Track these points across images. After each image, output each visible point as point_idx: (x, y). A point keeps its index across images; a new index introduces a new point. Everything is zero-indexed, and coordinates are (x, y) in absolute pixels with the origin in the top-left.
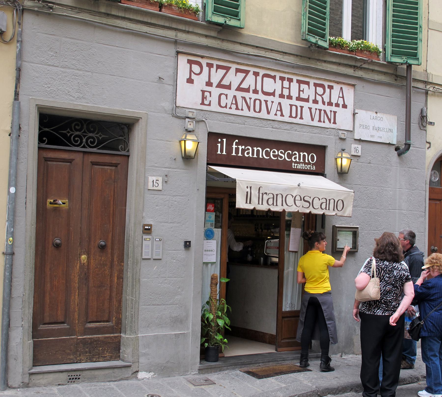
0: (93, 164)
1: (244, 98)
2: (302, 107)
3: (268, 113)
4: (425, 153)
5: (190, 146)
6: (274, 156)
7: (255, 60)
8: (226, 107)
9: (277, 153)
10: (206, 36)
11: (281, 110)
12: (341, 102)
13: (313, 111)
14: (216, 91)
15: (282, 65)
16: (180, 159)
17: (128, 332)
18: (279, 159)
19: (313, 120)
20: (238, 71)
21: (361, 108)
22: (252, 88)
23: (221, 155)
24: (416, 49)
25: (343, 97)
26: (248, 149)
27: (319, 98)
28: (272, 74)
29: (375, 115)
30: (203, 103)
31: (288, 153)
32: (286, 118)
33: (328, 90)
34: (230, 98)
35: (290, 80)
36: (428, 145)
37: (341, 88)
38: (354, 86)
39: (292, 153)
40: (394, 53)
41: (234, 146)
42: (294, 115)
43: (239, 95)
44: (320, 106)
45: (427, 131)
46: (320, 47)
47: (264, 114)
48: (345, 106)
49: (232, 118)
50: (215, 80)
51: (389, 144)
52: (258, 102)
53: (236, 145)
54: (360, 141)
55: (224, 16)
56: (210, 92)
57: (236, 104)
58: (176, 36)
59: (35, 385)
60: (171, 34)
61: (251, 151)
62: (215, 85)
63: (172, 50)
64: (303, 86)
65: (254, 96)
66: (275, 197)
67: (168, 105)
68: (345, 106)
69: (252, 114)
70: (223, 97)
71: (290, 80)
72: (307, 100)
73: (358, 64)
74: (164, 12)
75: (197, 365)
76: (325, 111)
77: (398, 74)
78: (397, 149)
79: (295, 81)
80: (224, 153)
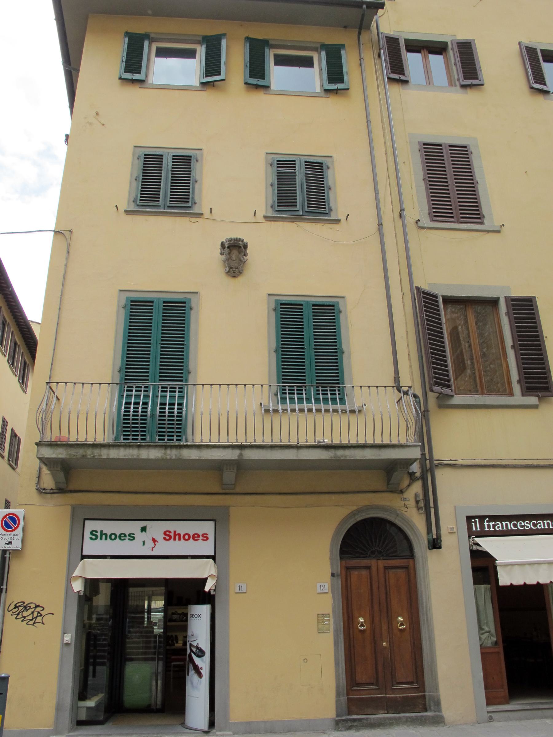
9: (523, 524)
18: (526, 528)
39: (537, 522)
41: (486, 523)
80: (478, 529)
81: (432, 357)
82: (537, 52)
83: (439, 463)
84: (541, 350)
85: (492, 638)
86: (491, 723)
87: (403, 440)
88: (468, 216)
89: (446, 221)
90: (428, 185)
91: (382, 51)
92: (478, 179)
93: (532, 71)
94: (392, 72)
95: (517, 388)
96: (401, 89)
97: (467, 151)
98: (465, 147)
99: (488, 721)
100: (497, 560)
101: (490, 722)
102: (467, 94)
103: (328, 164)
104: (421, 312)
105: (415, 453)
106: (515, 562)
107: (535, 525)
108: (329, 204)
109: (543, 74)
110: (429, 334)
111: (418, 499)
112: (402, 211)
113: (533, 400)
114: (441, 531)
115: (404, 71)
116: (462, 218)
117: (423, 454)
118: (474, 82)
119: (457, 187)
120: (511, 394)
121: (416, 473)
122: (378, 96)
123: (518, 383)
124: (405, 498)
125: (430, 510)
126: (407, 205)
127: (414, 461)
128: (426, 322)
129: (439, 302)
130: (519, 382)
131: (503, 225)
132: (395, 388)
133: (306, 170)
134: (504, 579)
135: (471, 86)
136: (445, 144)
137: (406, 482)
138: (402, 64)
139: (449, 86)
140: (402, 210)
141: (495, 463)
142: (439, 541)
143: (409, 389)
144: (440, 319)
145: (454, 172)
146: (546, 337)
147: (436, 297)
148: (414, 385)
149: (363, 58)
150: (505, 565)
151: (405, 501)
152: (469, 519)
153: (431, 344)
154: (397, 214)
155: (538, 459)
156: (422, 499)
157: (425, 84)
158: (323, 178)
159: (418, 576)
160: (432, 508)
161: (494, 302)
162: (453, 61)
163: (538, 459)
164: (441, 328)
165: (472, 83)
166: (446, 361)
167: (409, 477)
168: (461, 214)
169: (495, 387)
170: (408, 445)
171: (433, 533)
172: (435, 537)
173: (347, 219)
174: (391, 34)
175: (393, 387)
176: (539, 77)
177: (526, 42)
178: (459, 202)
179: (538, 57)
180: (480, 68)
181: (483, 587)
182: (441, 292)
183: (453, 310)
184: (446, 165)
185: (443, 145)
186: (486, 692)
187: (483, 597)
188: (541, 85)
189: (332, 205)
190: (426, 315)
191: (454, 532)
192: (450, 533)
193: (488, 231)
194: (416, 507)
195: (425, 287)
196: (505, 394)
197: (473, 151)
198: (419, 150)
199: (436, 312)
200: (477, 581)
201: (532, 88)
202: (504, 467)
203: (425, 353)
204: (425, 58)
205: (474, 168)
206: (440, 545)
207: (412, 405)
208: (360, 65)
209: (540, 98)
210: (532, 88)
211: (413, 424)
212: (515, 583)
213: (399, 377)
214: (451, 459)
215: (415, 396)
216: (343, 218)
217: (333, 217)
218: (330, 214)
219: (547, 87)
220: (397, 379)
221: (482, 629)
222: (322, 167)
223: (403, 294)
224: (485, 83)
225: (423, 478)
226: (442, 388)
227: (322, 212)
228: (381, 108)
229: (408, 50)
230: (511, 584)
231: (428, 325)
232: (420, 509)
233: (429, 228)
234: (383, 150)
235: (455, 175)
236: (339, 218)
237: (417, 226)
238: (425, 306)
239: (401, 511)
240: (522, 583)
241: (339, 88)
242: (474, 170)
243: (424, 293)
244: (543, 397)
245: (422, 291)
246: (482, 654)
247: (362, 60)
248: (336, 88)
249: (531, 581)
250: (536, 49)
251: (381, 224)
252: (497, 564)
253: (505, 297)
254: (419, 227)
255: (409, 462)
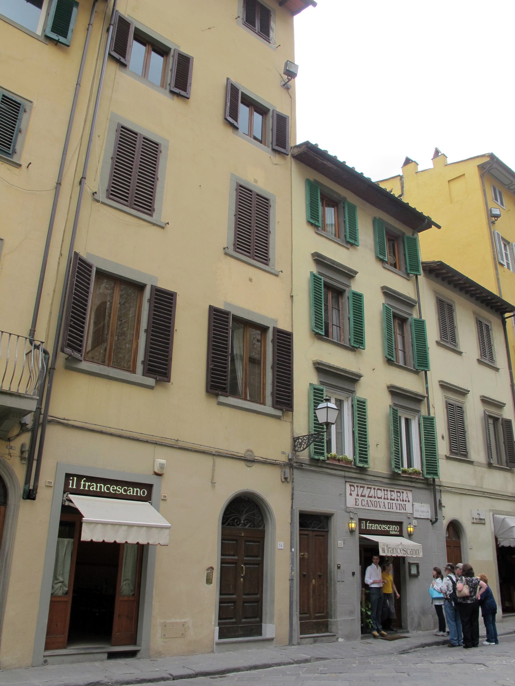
0: (316, 536)
1: (370, 501)
2: (392, 503)
3: (380, 507)
4: (442, 522)
5: (353, 525)
6: (113, 490)
7: (374, 482)
8: (364, 506)
9: (115, 489)
10: (355, 473)
11: (385, 506)
12: (407, 500)
13: (397, 504)
14: (360, 498)
15: (383, 483)
16: (349, 532)
17: (333, 618)
18: (117, 492)
19: (397, 509)
20: (368, 488)
21: (415, 502)
22: (373, 496)
23: (369, 529)
24: (437, 471)
25: (408, 497)
26: (93, 485)
27: (399, 498)
28: (380, 488)
29: (421, 504)
30: (356, 505)
31: (125, 489)
32: (387, 510)
33: (402, 494)
34: (366, 501)
35: (387, 491)
36: (443, 518)
37: (407, 493)
38: (411, 491)
39: (128, 488)
40: (428, 473)
41: (82, 483)
42: (390, 508)
43: (369, 499)
44: (399, 502)
45: (281, 481)
46: (397, 473)
47: (378, 508)
48: (409, 501)
49: (367, 511)
50: (360, 494)
51: (428, 519)
52: (376, 502)
53: (84, 482)
54: (416, 518)
55: (362, 463)
56: (358, 499)
57: (368, 504)
58: (345, 474)
59: (302, 644)
60: (342, 473)
61: (132, 491)
62: (360, 495)
63: (343, 480)
64: (392, 493)
65: (374, 500)
66: (393, 550)
67: (343, 507)
68: (409, 501)
69: (374, 508)
70: (363, 501)
71: (387, 491)
72: (394, 500)
73: (414, 480)
74: (341, 464)
75: (360, 635)
76: (401, 504)
77: (429, 483)
78: (431, 521)
79: (389, 491)
80: (74, 487)
81: (71, 320)
82: (238, 92)
83: (53, 420)
84: (168, 340)
85: (64, 587)
86: (45, 666)
87: (22, 391)
88: (141, 205)
89: (121, 202)
90: (114, 165)
91: (112, 27)
92: (159, 177)
93: (230, 106)
94: (115, 51)
95: (140, 368)
96: (118, 70)
97: (157, 148)
98: (157, 145)
99: (43, 664)
100: (84, 517)
101: (44, 665)
102: (173, 100)
103: (26, 107)
104: (73, 277)
105: (32, 405)
106: (99, 521)
107: (125, 491)
108: (14, 146)
109: (237, 112)
110: (74, 298)
111: (23, 450)
112: (83, 179)
113: (150, 381)
114: (38, 483)
115: (125, 55)
116: (135, 204)
117: (39, 409)
118: (183, 93)
119: (139, 176)
120: (134, 372)
121: (28, 424)
122: (27, 33)
123: (142, 363)
124: (12, 447)
125: (33, 461)
126: (90, 176)
127: (28, 412)
128: (74, 286)
129: (92, 272)
130: (143, 362)
131: (168, 223)
132: (28, 340)
133: (1, 104)
134: (86, 535)
135: (178, 95)
136: (140, 134)
137: (16, 431)
138: (126, 47)
139: (160, 86)
140: (84, 178)
141: (104, 429)
142: (34, 492)
143: (41, 344)
144: (88, 288)
145: (141, 162)
146: (176, 330)
147: (91, 267)
148: (47, 342)
149: (91, 25)
150: (90, 523)
151: (10, 450)
152: (68, 476)
153: (73, 308)
154: (78, 180)
155: (142, 434)
156: (28, 451)
157: (141, 75)
158: (16, 119)
159: (6, 523)
160: (35, 460)
161: (140, 287)
162: (170, 67)
163: (142, 434)
164: (87, 297)
165: (180, 93)
166: (83, 328)
167: (20, 428)
168: (136, 201)
169: (126, 365)
170: (26, 396)
171: (31, 484)
172: (31, 488)
173: (28, 167)
174: (125, 17)
175: (26, 338)
176: (234, 113)
177: (233, 80)
178: (137, 190)
179: (238, 97)
180: (191, 83)
181: (66, 541)
182: (96, 264)
183: (108, 286)
184: (136, 154)
185: (139, 135)
186: (47, 638)
187: (65, 550)
188: (233, 121)
189: (18, 148)
190: (77, 281)
191: (52, 486)
192: (47, 486)
193: (154, 224)
194: (20, 457)
195: (83, 254)
196: (127, 371)
197: (162, 151)
198: (116, 131)
199: (87, 280)
200: (61, 535)
201: (226, 119)
202: (111, 435)
203: (66, 315)
204: (148, 54)
205: (158, 166)
206: (34, 496)
207: (40, 359)
208: (88, 29)
209: (229, 131)
210: (226, 119)
211: (36, 378)
212: (95, 540)
213: (35, 331)
214: (64, 418)
215: (45, 352)
216: (24, 165)
217: (15, 159)
218: (13, 156)
219: (238, 124)
220: (32, 332)
221: (57, 579)
222: (19, 107)
223: (61, 255)
224: (191, 98)
225: (34, 431)
226: (73, 351)
227: (6, 150)
228: (94, 78)
229: (136, 38)
230: (92, 540)
231: (76, 289)
232: (23, 460)
233: (103, 203)
234: (84, 117)
235: (140, 165)
236: (21, 163)
237: (93, 197)
238: (78, 272)
239: (3, 458)
240: (101, 540)
241: (60, 41)
242: (158, 167)
243: (80, 259)
244: (160, 380)
245: (79, 258)
246: (52, 602)
247: (90, 26)
248: (57, 39)
249: (110, 539)
250: (238, 90)
251: (60, 184)
252: (83, 521)
253: (152, 286)
254: (94, 199)
255: (24, 413)
